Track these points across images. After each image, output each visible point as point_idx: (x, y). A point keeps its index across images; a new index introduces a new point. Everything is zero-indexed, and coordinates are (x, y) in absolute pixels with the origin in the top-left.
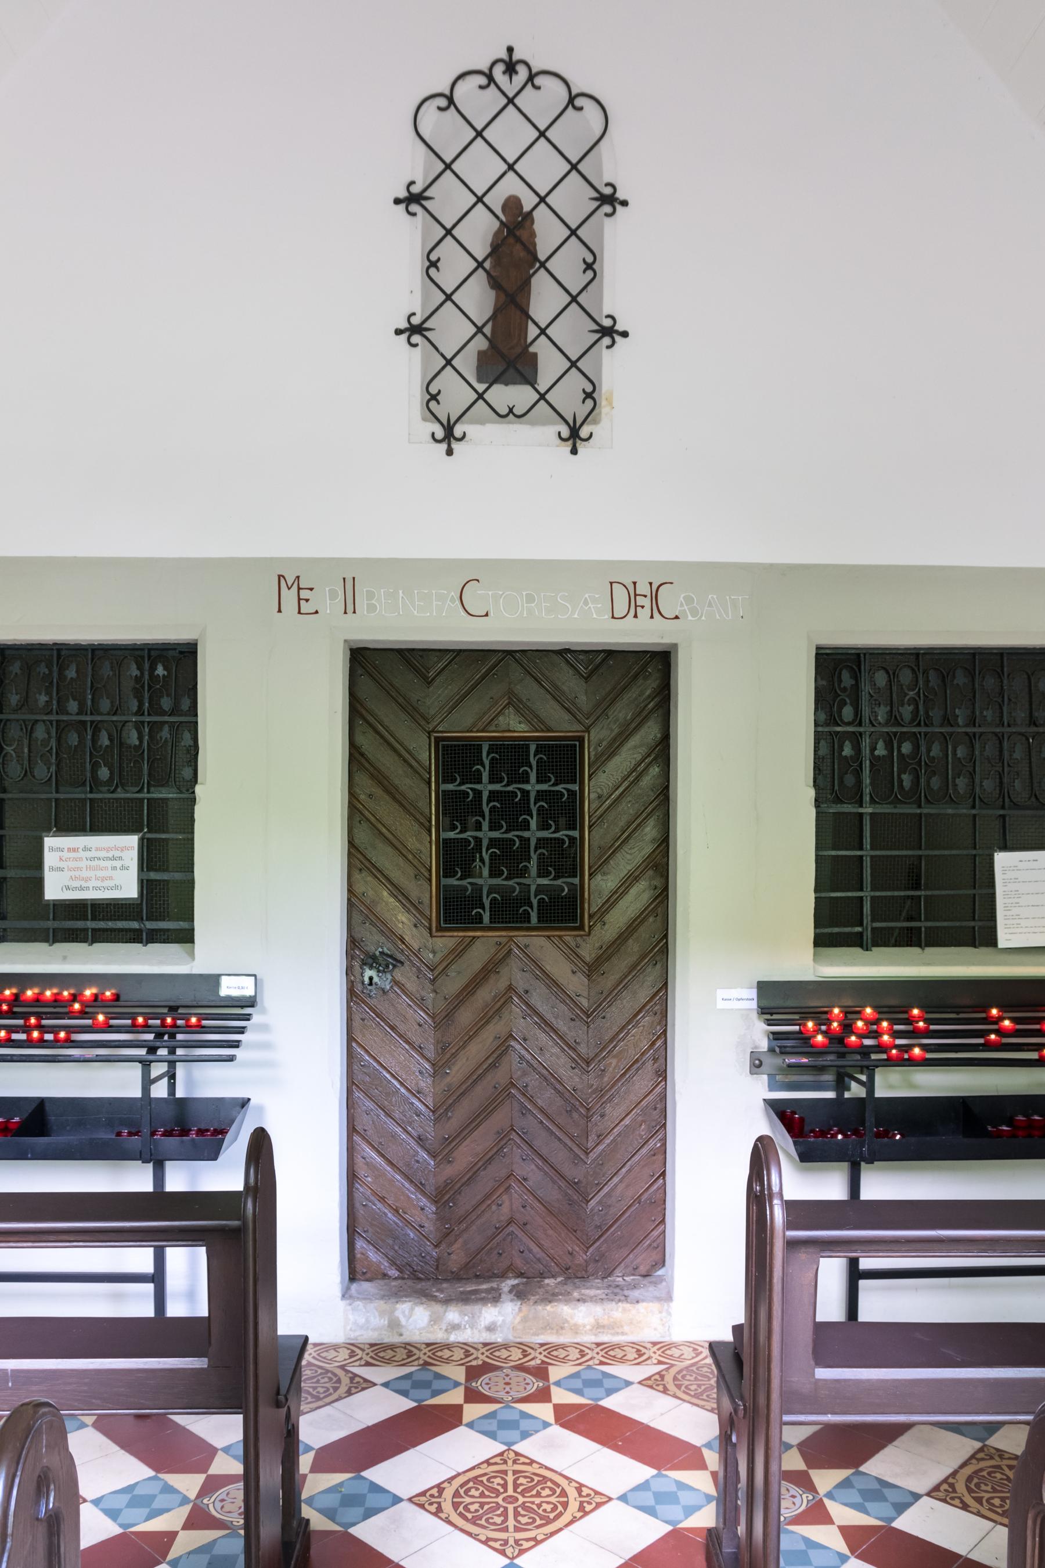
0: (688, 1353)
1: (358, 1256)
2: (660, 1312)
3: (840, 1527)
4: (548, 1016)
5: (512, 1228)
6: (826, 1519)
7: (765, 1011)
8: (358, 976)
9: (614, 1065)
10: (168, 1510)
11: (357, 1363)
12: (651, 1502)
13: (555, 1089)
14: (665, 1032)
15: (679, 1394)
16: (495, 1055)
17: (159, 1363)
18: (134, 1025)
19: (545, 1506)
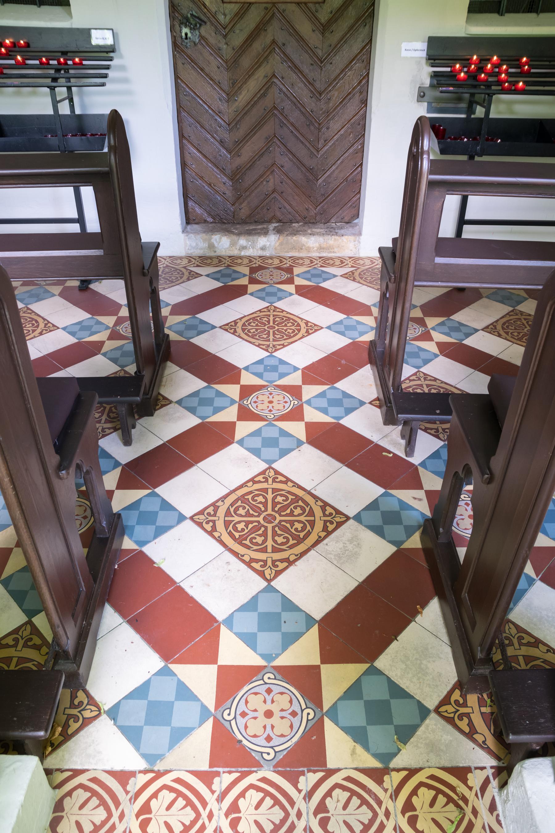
0: (368, 262)
1: (190, 210)
2: (354, 241)
3: (436, 342)
4: (297, 62)
5: (275, 195)
6: (430, 339)
7: (432, 59)
8: (178, 32)
9: (336, 95)
10: (99, 332)
11: (192, 266)
12: (343, 330)
13: (300, 110)
14: (368, 74)
15: (361, 281)
16: (265, 88)
17: (77, 252)
18: (42, 63)
19: (289, 330)
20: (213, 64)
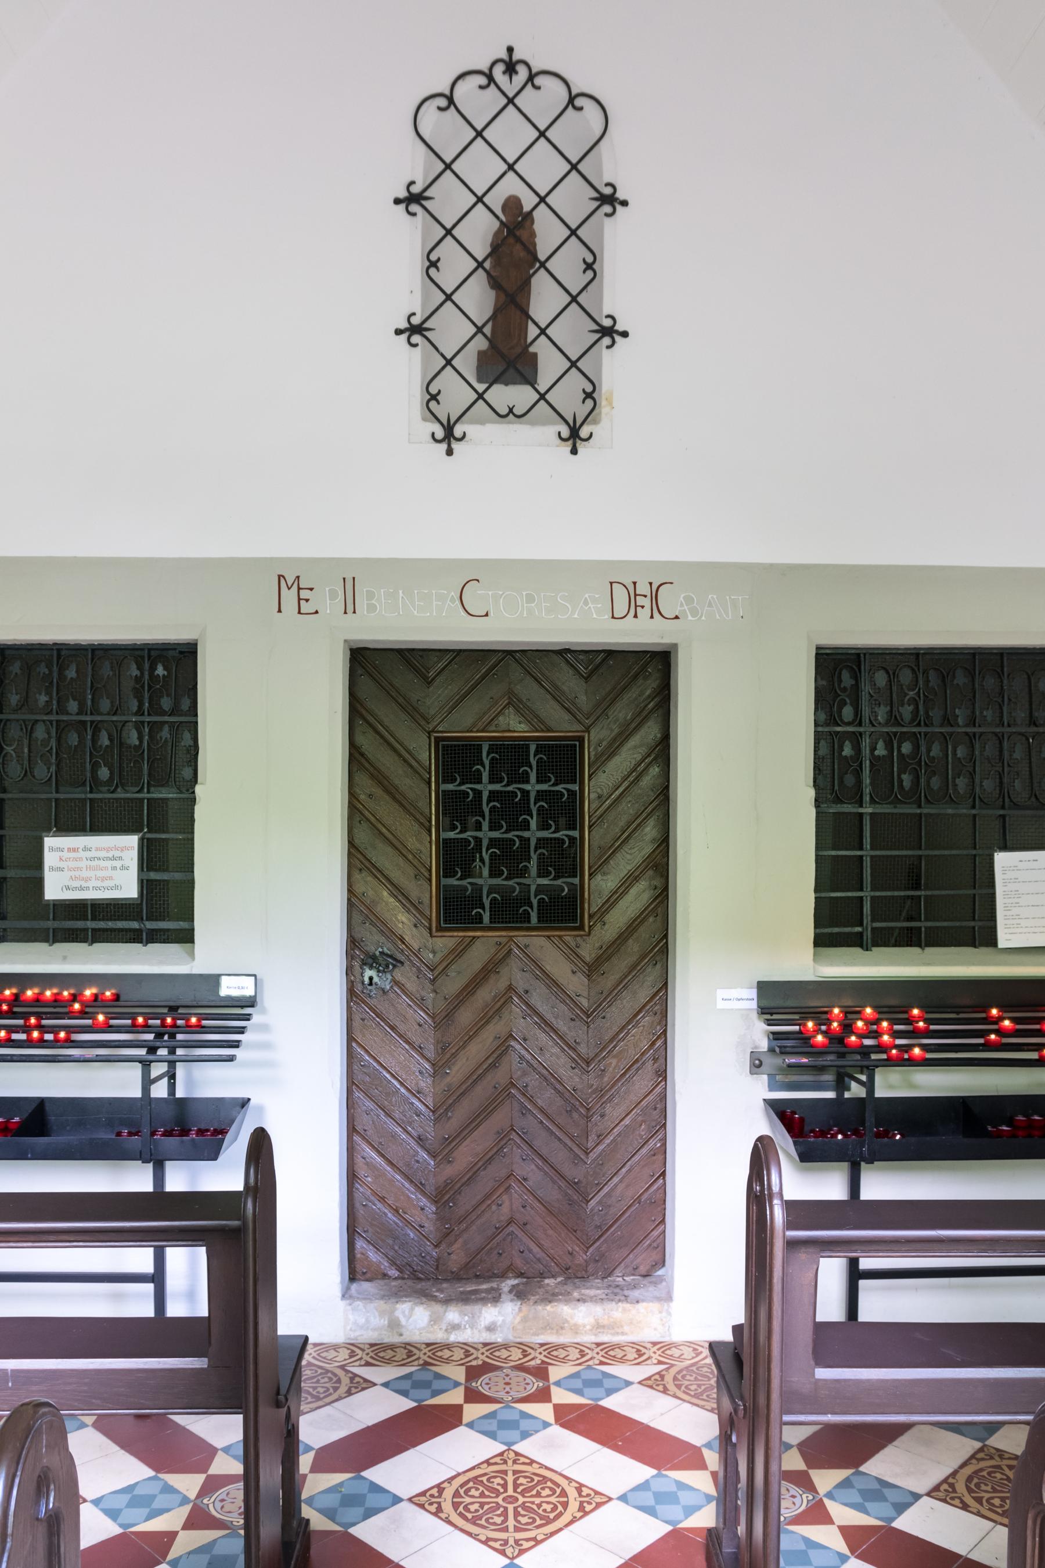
0: (688, 1353)
1: (358, 1256)
2: (660, 1312)
3: (840, 1527)
4: (548, 1016)
5: (512, 1228)
6: (826, 1519)
7: (765, 1011)
8: (358, 976)
9: (614, 1065)
10: (168, 1510)
11: (357, 1363)
12: (651, 1502)
13: (555, 1089)
14: (665, 1032)
15: (679, 1394)
16: (495, 1055)
17: (159, 1363)
18: (134, 1025)
19: (545, 1506)
20: (414, 1019)
